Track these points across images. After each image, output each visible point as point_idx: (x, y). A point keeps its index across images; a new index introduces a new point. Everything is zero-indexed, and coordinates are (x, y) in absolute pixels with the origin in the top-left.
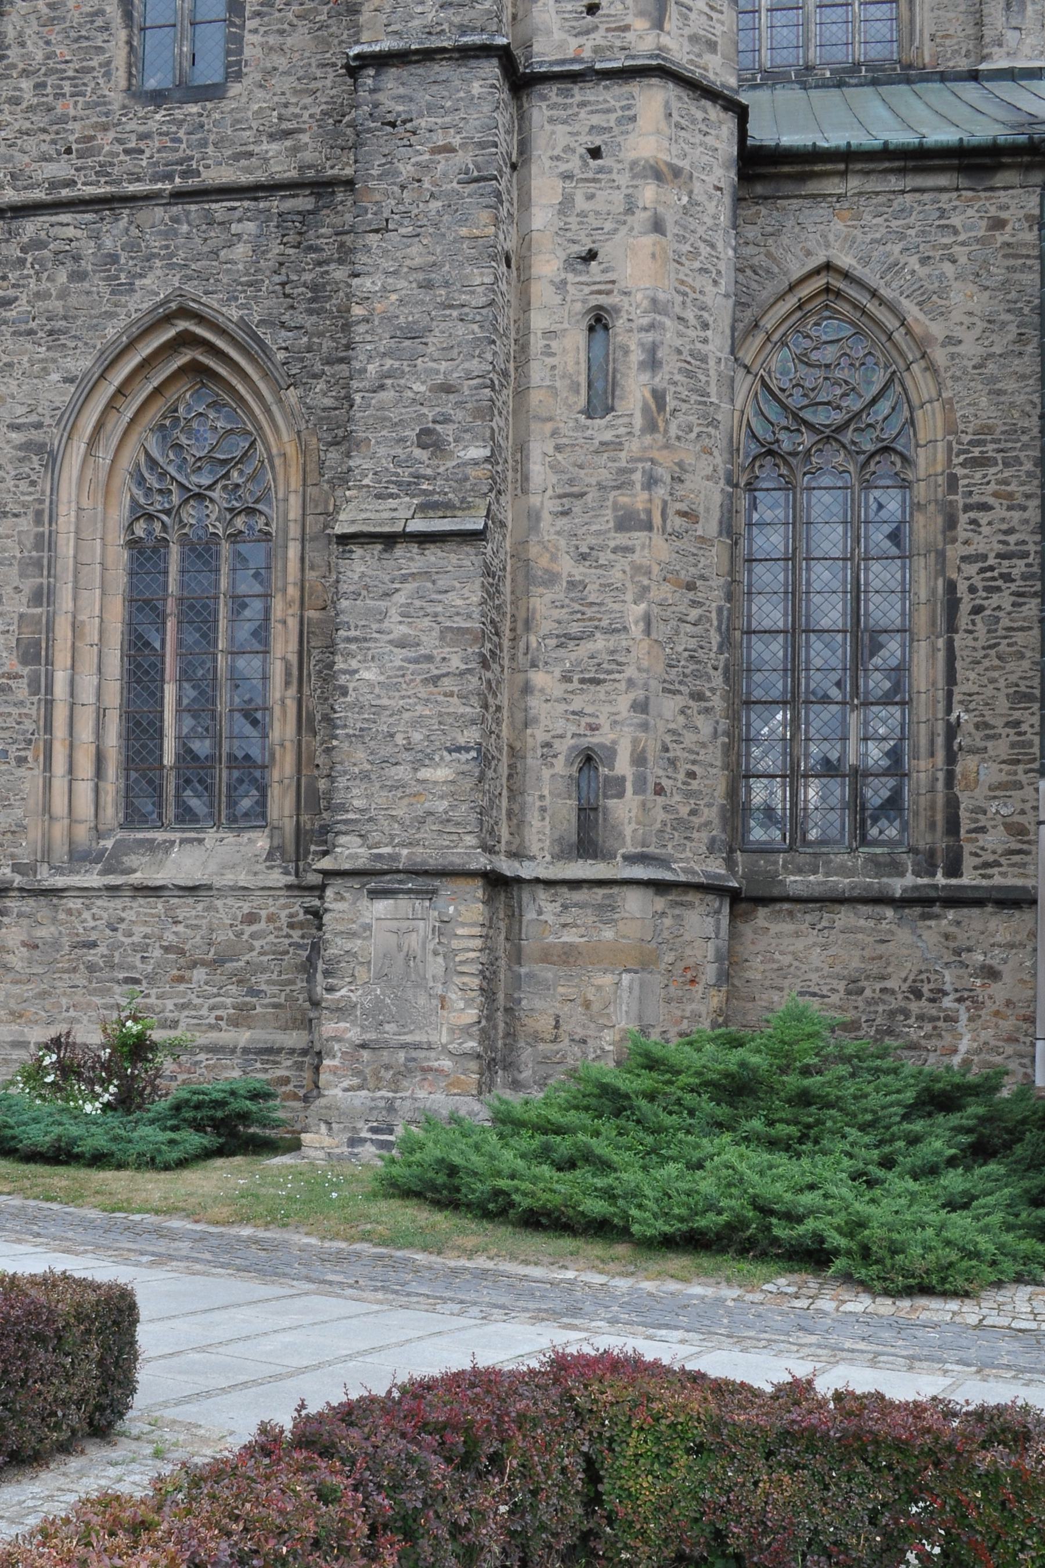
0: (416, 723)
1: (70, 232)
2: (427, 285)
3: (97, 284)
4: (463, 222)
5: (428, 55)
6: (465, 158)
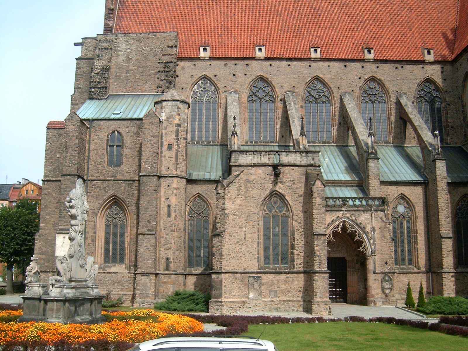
0: (147, 256)
1: (99, 184)
2: (149, 203)
3: (103, 191)
4: (153, 195)
5: (149, 176)
6: (153, 188)
